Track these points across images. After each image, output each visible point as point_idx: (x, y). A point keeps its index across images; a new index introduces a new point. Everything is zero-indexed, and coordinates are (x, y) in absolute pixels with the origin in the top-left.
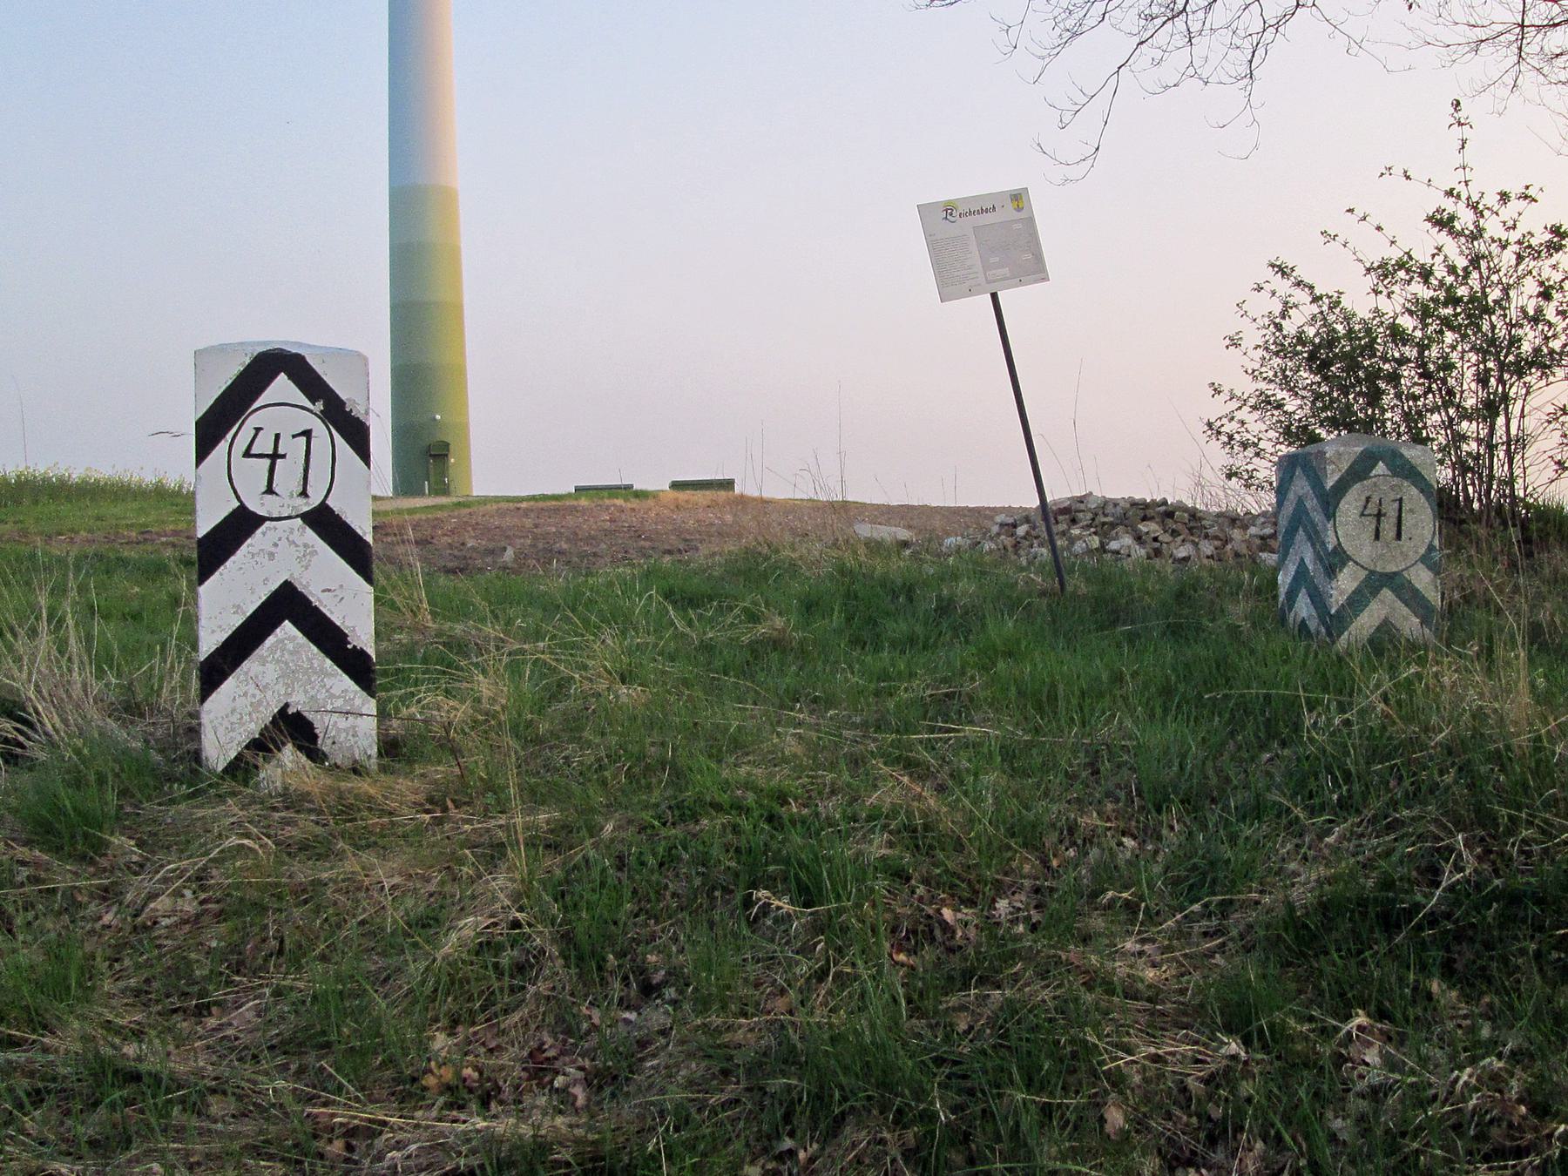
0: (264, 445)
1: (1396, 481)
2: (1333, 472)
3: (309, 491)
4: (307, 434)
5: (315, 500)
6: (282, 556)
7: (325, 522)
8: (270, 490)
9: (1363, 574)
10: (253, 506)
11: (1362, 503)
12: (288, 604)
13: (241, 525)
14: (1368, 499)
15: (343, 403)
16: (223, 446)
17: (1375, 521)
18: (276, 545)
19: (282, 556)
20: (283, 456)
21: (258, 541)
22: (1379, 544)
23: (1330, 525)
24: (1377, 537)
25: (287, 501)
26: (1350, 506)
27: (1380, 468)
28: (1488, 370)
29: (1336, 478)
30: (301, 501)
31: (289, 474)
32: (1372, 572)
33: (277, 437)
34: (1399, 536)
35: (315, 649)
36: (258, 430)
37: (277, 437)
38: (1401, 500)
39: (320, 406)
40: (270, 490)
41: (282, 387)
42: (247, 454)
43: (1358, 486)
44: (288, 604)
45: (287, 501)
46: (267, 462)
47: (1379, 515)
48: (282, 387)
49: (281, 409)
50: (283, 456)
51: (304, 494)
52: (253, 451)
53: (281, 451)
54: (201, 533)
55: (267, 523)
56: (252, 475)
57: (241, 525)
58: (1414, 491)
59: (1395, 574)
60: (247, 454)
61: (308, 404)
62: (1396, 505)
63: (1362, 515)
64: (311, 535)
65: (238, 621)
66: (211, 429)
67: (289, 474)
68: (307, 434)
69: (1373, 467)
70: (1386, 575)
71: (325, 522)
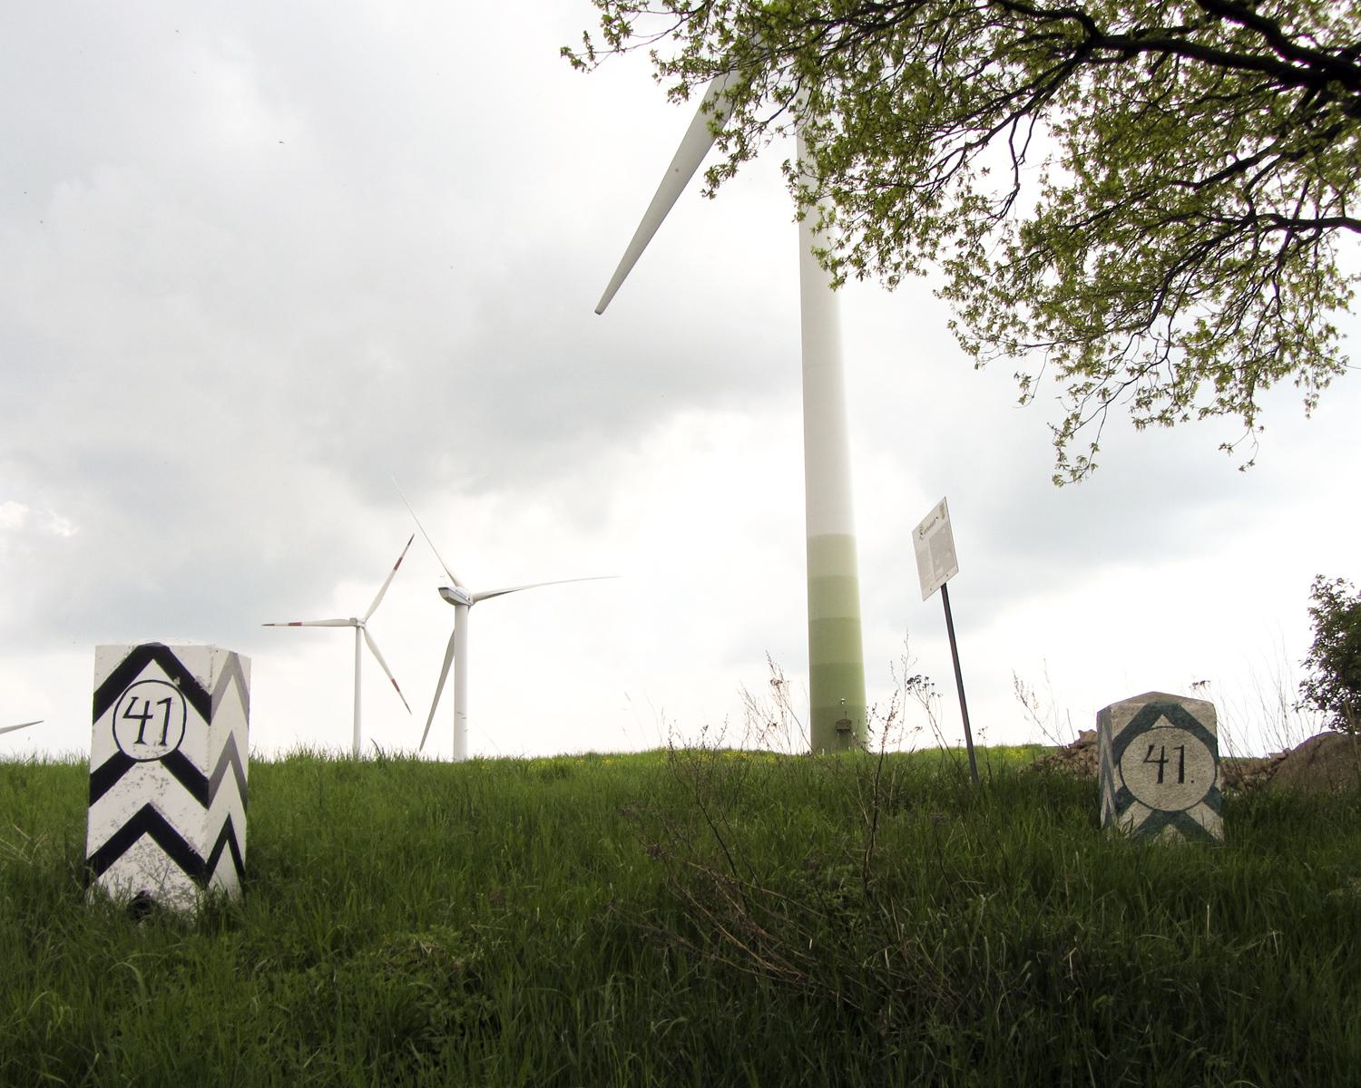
0: (138, 709)
1: (1178, 731)
2: (1118, 723)
3: (145, 738)
4: (168, 701)
5: (171, 747)
6: (147, 786)
7: (178, 764)
8: (140, 741)
9: (1147, 813)
10: (130, 751)
11: (197, 669)
12: (148, 821)
13: (119, 765)
14: (1151, 748)
15: (1040, 745)
16: (111, 710)
17: (1157, 767)
18: (142, 779)
19: (147, 786)
20: (151, 717)
21: (132, 774)
22: (1161, 786)
23: (1116, 770)
24: (1160, 780)
25: (152, 749)
26: (1135, 751)
27: (1162, 721)
28: (981, 965)
29: (1120, 730)
30: (162, 748)
31: (154, 728)
32: (1155, 811)
33: (148, 703)
34: (1181, 779)
35: (164, 854)
36: (135, 699)
37: (148, 703)
38: (1182, 748)
39: (176, 682)
40: (140, 741)
41: (153, 670)
42: (127, 716)
43: (1140, 737)
44: (148, 821)
45: (152, 748)
46: (139, 721)
47: (1162, 762)
48: (153, 670)
49: (152, 685)
50: (151, 717)
51: (163, 743)
52: (131, 714)
53: (149, 713)
54: (92, 771)
55: (137, 764)
56: (128, 730)
57: (119, 765)
58: (1194, 740)
59: (1179, 812)
60: (127, 716)
61: (168, 679)
62: (1178, 753)
63: (1146, 761)
64: (166, 773)
65: (113, 831)
66: (105, 697)
67: (154, 728)
68: (168, 701)
69: (1156, 719)
70: (1169, 813)
71: (178, 764)
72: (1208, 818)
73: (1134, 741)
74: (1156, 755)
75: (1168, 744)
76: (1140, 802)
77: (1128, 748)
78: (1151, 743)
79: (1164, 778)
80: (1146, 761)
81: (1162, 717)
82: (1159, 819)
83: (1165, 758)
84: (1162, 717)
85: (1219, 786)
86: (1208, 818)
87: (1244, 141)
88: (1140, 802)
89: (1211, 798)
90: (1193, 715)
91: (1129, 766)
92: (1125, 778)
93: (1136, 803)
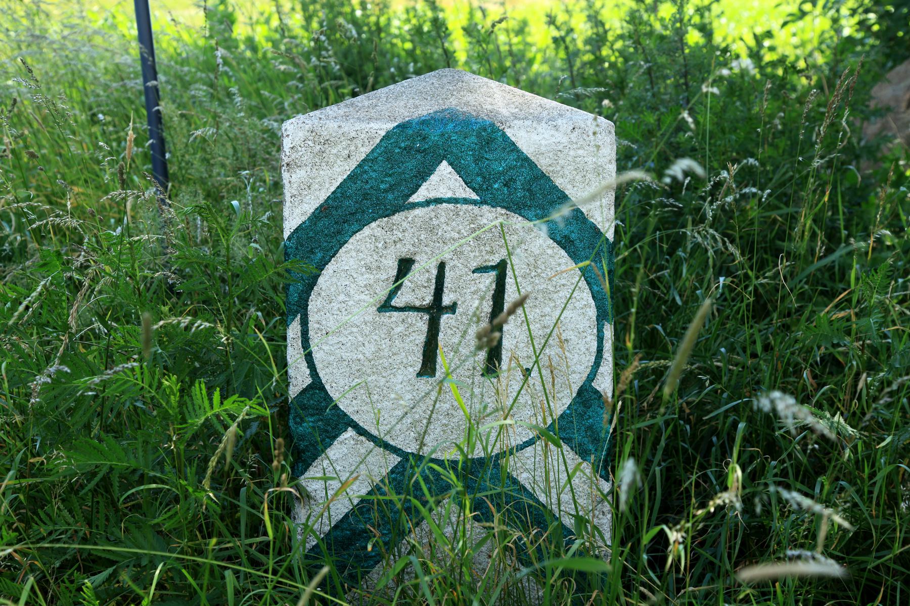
1: (491, 216)
9: (382, 464)
14: (405, 265)
27: (444, 180)
32: (407, 461)
38: (501, 269)
43: (373, 229)
47: (436, 309)
50: (452, 308)
62: (488, 281)
63: (386, 306)
69: (424, 174)
72: (567, 484)
73: (353, 243)
74: (417, 289)
75: (457, 253)
76: (361, 431)
77: (330, 268)
78: (404, 250)
79: (441, 360)
80: (386, 306)
81: (444, 168)
82: (412, 481)
83: (446, 300)
84: (444, 168)
85: (605, 384)
86: (567, 484)
87: (174, 378)
88: (361, 431)
89: (576, 426)
90: (543, 164)
91: (331, 325)
92: (317, 356)
93: (350, 433)
